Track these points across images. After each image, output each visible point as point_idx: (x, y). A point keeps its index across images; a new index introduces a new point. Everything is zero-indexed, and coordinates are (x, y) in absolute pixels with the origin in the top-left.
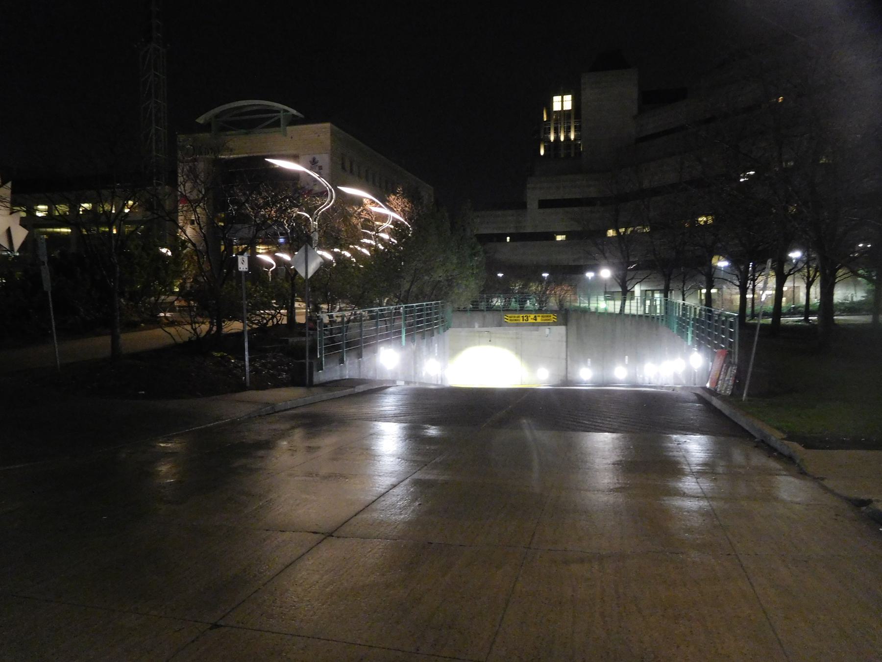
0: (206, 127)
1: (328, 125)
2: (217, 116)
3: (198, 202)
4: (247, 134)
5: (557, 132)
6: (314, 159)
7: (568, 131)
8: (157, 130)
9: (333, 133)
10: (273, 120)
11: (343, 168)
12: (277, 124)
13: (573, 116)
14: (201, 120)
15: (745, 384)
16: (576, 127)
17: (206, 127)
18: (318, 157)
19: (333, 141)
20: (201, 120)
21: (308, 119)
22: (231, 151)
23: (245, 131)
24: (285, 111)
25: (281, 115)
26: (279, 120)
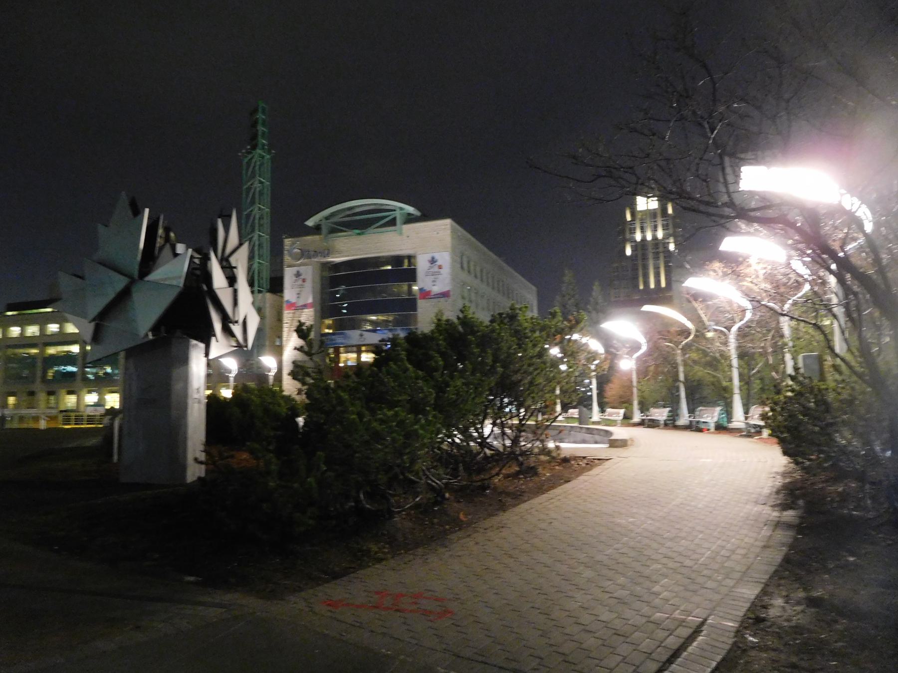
0: (317, 229)
1: (447, 223)
2: (327, 218)
3: (725, 205)
4: (359, 234)
5: (643, 230)
6: (433, 258)
7: (655, 229)
8: (260, 236)
9: (453, 231)
10: (387, 219)
11: (462, 268)
12: (393, 222)
13: (659, 215)
14: (310, 223)
15: (678, 396)
16: (663, 226)
17: (317, 229)
18: (437, 256)
19: (453, 238)
20: (310, 223)
21: (425, 217)
22: (340, 253)
23: (357, 231)
24: (401, 209)
25: (397, 214)
26: (394, 219)
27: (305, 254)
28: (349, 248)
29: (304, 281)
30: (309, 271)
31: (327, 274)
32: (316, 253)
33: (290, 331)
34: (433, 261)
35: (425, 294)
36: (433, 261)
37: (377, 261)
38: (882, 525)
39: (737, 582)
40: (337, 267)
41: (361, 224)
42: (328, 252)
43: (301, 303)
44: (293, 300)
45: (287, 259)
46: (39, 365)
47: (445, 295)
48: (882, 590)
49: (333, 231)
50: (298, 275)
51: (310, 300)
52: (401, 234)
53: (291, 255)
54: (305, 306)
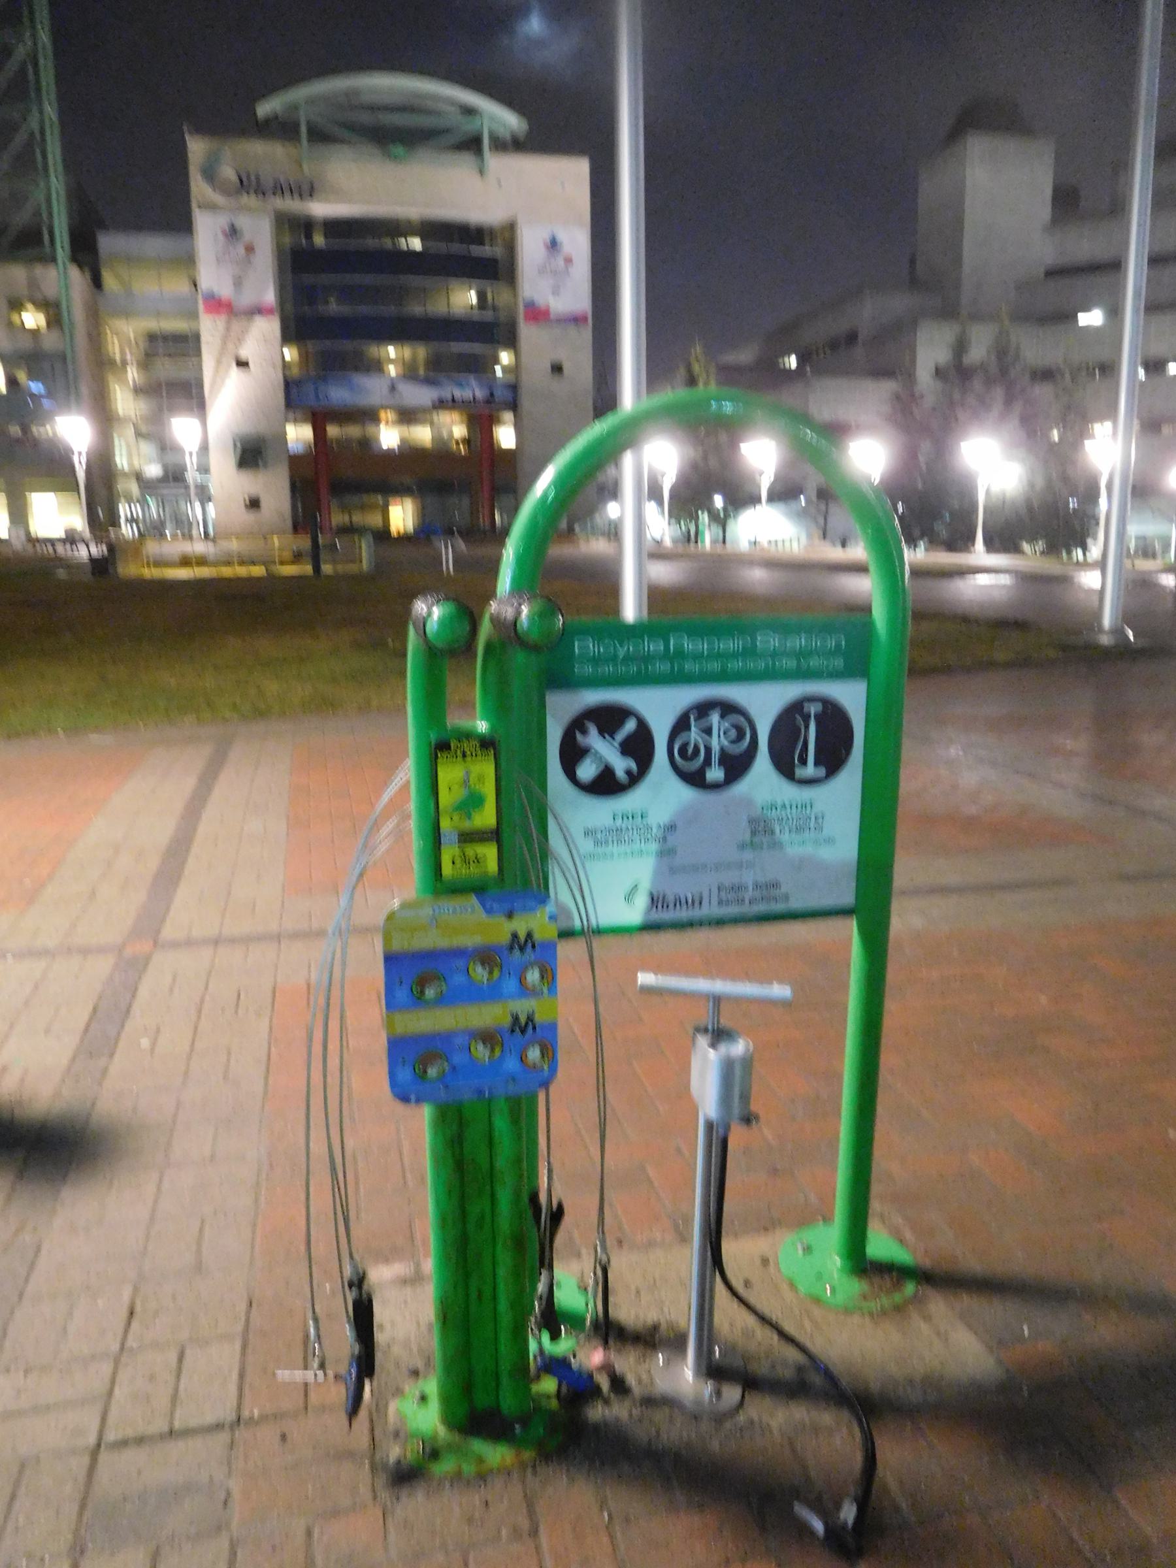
0: (282, 129)
12: (472, 145)
14: (265, 109)
18: (563, 237)
20: (265, 109)
22: (338, 194)
27: (248, 184)
28: (357, 188)
29: (250, 249)
30: (260, 231)
31: (287, 240)
32: (279, 189)
33: (219, 362)
34: (553, 244)
35: (537, 314)
36: (553, 244)
37: (397, 228)
38: (576, 1125)
39: (117, 1362)
40: (306, 225)
41: (397, 134)
42: (309, 190)
43: (246, 299)
44: (225, 290)
45: (199, 187)
46: (308, 279)
47: (577, 320)
48: (415, 1350)
49: (320, 136)
50: (233, 233)
51: (270, 297)
52: (481, 172)
53: (210, 174)
54: (260, 310)
